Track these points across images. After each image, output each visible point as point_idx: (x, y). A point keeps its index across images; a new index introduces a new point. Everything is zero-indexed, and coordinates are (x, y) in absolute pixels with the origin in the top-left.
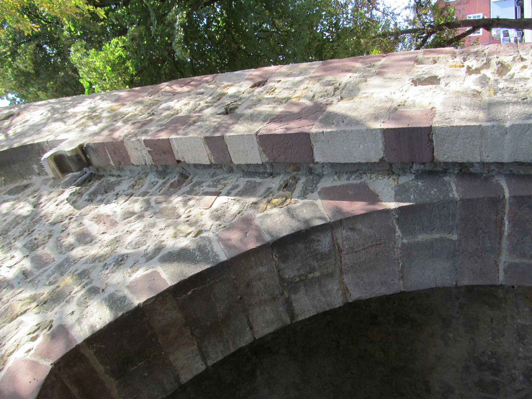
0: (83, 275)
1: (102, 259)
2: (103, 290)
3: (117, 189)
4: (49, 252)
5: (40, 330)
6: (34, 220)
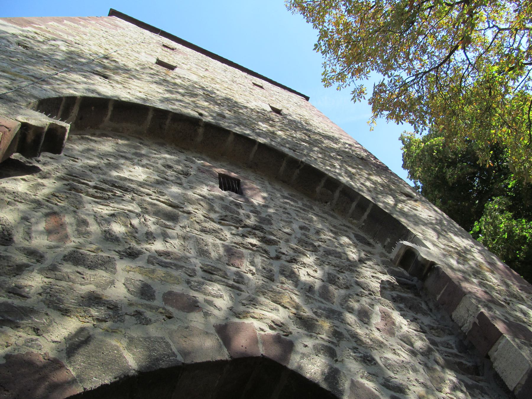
0: (337, 334)
1: (359, 342)
2: (337, 361)
3: (419, 316)
4: (336, 295)
5: (281, 328)
6: (351, 267)
